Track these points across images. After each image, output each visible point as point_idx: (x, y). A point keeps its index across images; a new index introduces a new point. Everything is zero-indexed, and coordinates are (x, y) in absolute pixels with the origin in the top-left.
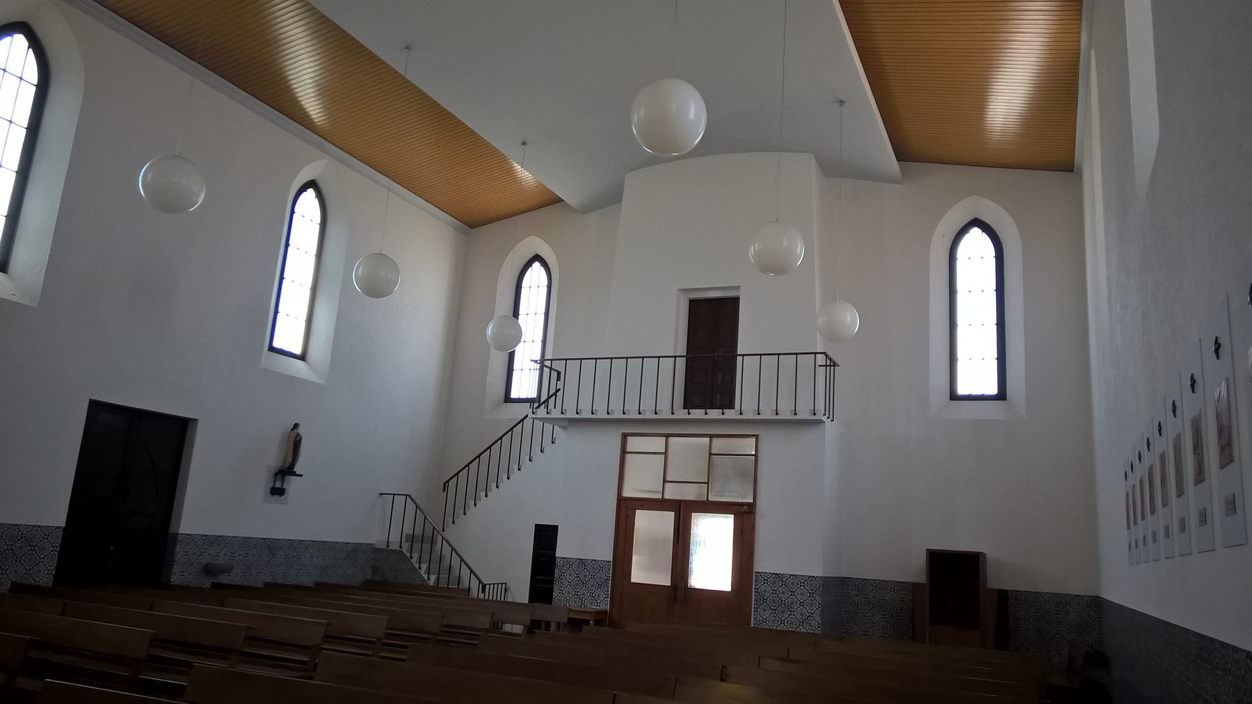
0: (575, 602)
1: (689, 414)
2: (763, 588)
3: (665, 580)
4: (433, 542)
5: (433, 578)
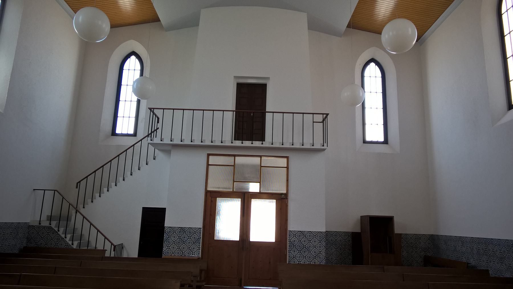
0: (178, 253)
1: (242, 143)
2: (293, 239)
3: (236, 237)
4: (68, 219)
5: (76, 243)
